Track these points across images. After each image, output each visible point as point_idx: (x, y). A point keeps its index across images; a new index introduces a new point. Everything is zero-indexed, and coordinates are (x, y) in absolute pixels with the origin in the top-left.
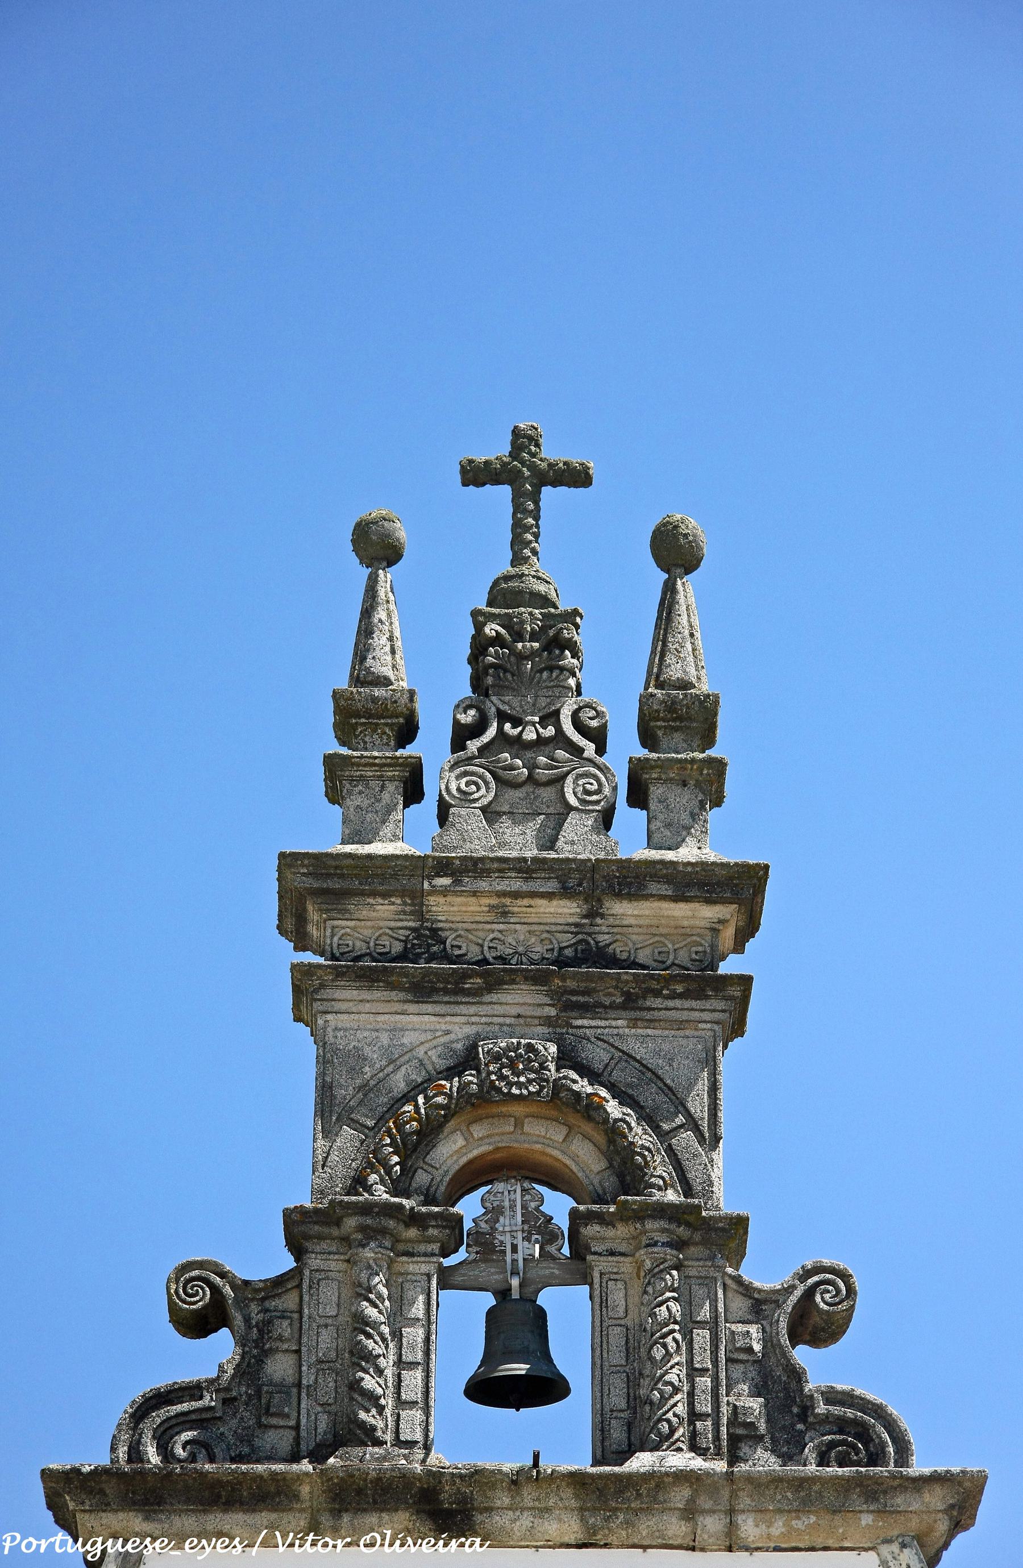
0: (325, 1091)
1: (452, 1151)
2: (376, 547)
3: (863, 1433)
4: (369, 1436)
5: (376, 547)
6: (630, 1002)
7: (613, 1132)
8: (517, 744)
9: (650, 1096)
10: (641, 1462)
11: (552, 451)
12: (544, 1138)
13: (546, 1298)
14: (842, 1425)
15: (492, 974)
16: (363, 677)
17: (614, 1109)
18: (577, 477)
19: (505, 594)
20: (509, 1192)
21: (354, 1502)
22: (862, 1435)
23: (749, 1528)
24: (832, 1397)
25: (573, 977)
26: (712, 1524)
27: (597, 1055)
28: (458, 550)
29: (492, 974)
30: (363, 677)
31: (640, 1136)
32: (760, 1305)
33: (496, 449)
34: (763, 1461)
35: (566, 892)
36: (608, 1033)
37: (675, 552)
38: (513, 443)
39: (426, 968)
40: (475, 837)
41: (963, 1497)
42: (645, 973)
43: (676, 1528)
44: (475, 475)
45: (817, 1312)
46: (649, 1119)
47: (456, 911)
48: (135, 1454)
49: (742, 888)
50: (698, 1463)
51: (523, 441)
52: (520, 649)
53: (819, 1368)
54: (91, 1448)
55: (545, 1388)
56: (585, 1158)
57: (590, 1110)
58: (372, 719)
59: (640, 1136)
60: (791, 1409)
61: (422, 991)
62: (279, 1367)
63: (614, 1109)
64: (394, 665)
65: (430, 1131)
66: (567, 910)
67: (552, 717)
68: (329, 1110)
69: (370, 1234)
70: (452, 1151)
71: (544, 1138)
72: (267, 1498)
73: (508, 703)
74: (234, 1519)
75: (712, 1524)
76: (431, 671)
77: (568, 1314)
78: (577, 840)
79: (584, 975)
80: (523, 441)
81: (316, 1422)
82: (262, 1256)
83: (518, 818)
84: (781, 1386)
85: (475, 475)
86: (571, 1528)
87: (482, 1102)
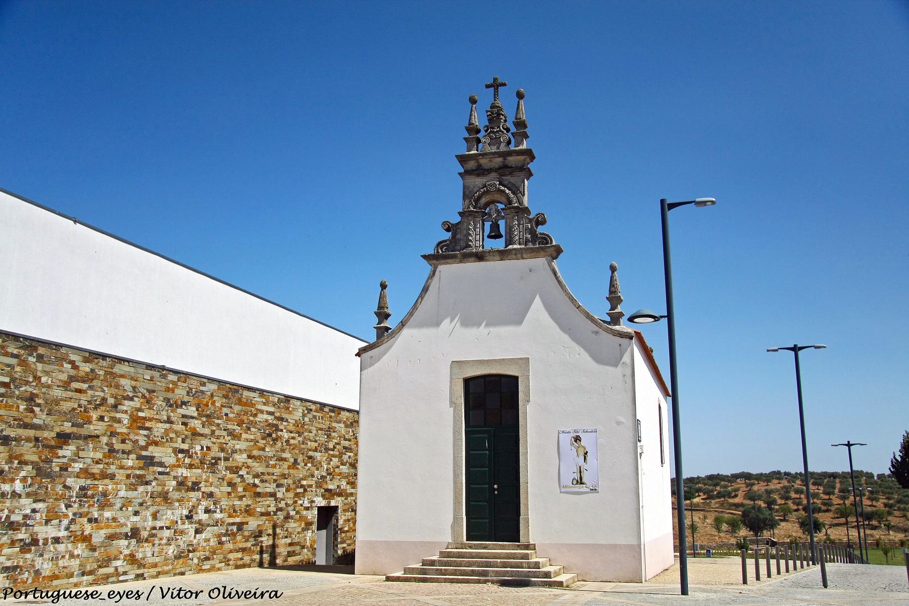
0: (464, 192)
1: (483, 201)
2: (473, 101)
3: (545, 239)
4: (470, 246)
5: (473, 101)
6: (511, 174)
7: (507, 195)
8: (493, 132)
9: (514, 189)
10: (510, 247)
11: (500, 81)
12: (497, 197)
13: (499, 222)
14: (542, 238)
15: (490, 171)
16: (470, 124)
17: (507, 191)
18: (505, 85)
19: (493, 106)
20: (492, 206)
21: (466, 257)
22: (546, 239)
23: (525, 256)
24: (541, 234)
25: (501, 171)
26: (519, 256)
27: (506, 183)
28: (486, 98)
29: (490, 171)
30: (470, 124)
31: (512, 195)
32: (530, 221)
33: (491, 81)
34: (530, 245)
35: (500, 156)
36: (507, 179)
37: (520, 96)
38: (825, 475)
39: (480, 171)
40: (488, 149)
41: (558, 251)
42: (515, 168)
43: (514, 257)
44: (488, 86)
45: (540, 221)
46: (513, 193)
47: (484, 161)
48: (438, 252)
49: (529, 153)
50: (519, 247)
51: (495, 79)
52: (495, 115)
53: (540, 229)
54: (431, 251)
55: (500, 236)
56: (504, 199)
57: (504, 192)
58: (473, 130)
59: (512, 195)
60: (535, 237)
61: (478, 175)
62: (458, 236)
63: (507, 191)
64: (476, 121)
65: (479, 198)
66: (501, 159)
67: (499, 127)
68: (465, 197)
69: (470, 215)
70: (483, 201)
71: (497, 197)
72: (453, 257)
73: (492, 125)
74: (449, 261)
75: (519, 256)
76: (480, 120)
77: (502, 224)
78: (503, 148)
79: (504, 170)
80: (495, 79)
81: (463, 244)
82: (456, 219)
83: (494, 145)
84: (533, 232)
85: (488, 86)
86: (499, 258)
87: (487, 192)
